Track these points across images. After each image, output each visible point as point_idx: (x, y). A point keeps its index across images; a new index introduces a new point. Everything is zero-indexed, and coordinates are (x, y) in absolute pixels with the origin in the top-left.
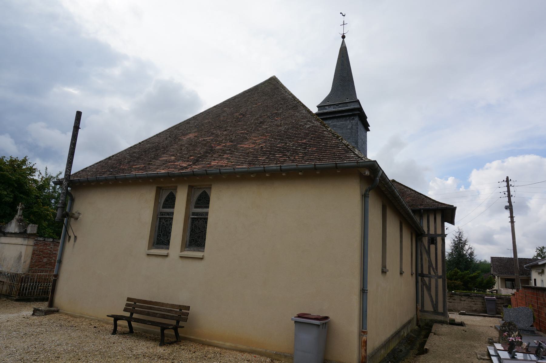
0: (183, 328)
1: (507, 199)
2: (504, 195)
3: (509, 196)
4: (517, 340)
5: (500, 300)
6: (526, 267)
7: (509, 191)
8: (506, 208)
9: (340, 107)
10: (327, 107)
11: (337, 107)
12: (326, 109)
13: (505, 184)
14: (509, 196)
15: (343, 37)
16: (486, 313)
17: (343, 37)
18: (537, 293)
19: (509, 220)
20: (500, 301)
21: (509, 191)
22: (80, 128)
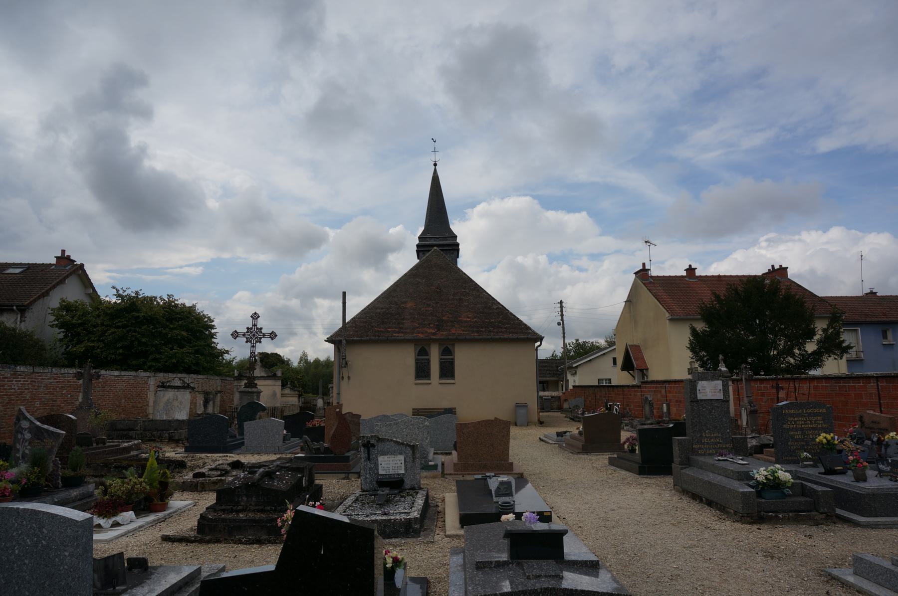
0: (445, 465)
1: (560, 318)
2: (558, 315)
3: (562, 315)
4: (798, 401)
5: (553, 399)
6: (560, 369)
7: (562, 311)
8: (559, 324)
9: (440, 241)
10: (428, 239)
11: (438, 240)
12: (427, 241)
13: (559, 305)
14: (562, 315)
15: (435, 165)
16: (543, 410)
17: (435, 165)
18: (796, 400)
19: (562, 335)
20: (553, 399)
21: (562, 311)
22: (63, 251)
